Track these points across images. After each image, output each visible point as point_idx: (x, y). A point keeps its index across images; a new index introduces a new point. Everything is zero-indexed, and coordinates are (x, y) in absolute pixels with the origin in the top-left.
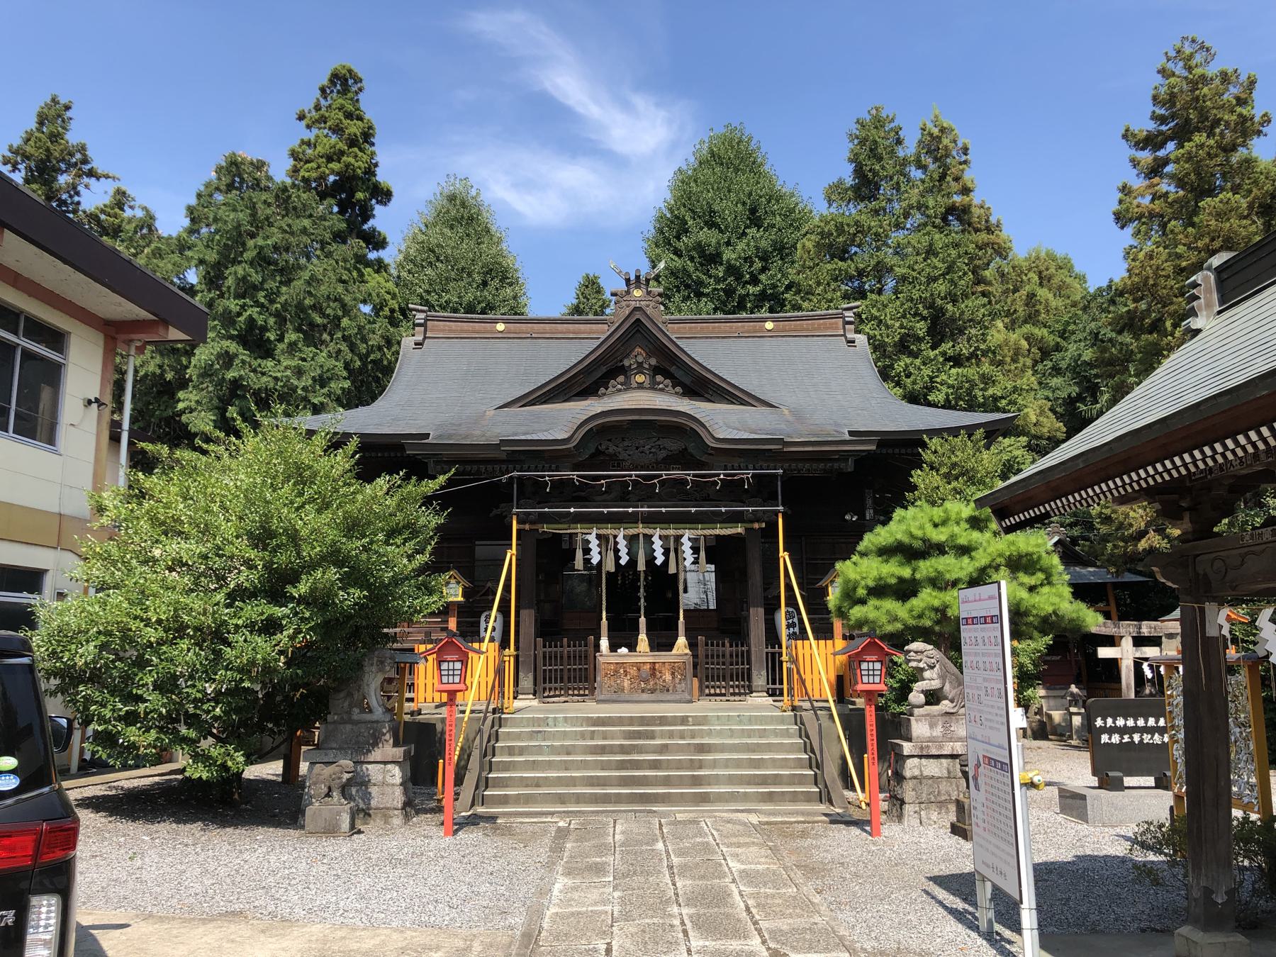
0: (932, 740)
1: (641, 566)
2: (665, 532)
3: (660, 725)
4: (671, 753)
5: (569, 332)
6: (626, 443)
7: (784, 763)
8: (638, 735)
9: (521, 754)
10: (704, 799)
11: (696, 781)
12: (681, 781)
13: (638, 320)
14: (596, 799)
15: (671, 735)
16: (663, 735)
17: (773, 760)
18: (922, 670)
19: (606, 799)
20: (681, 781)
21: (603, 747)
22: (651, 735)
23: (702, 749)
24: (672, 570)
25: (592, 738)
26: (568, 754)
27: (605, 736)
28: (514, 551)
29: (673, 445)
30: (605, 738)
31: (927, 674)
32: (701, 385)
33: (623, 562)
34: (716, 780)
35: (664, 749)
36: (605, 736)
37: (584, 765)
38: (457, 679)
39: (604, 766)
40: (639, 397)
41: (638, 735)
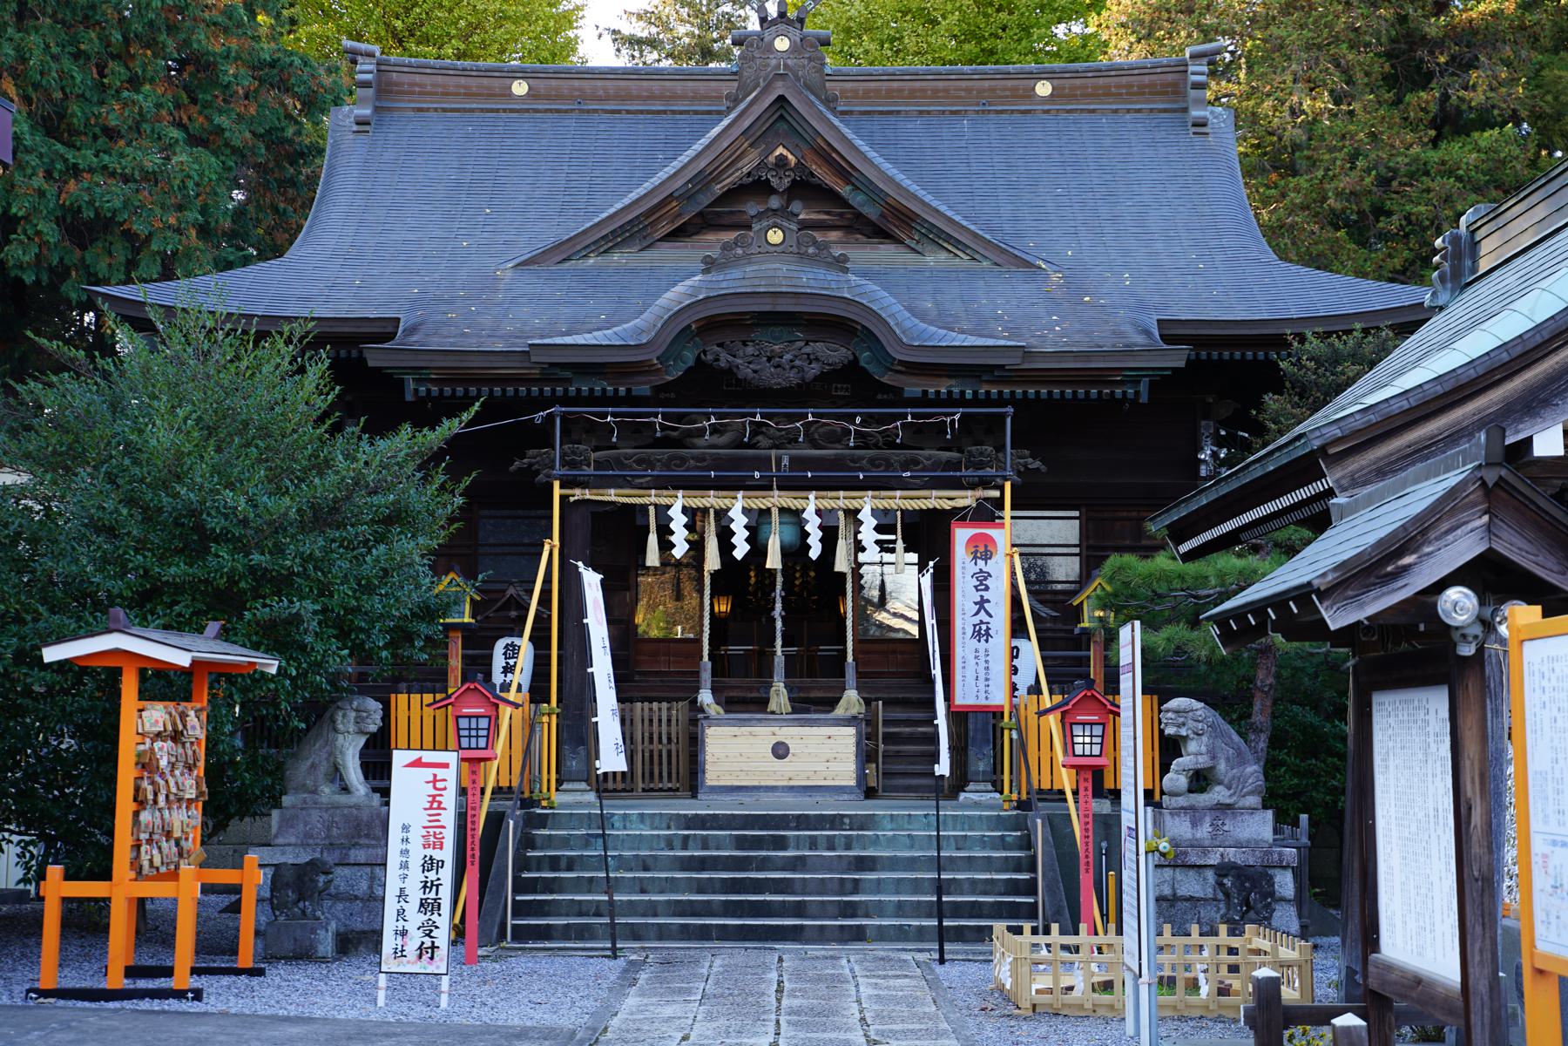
0: (1195, 844)
1: (774, 561)
2: (827, 504)
3: (797, 828)
4: (804, 870)
5: (652, 97)
6: (750, 350)
7: (988, 887)
8: (757, 843)
9: (570, 869)
10: (858, 935)
11: (849, 910)
12: (823, 910)
13: (781, 98)
14: (686, 933)
15: (813, 843)
16: (798, 843)
17: (973, 882)
18: (1186, 738)
19: (704, 934)
20: (823, 910)
21: (703, 859)
22: (780, 843)
23: (863, 864)
24: (842, 564)
25: (685, 848)
26: (646, 869)
27: (705, 843)
28: (556, 541)
29: (832, 353)
30: (705, 847)
31: (1192, 746)
32: (891, 223)
33: (739, 553)
34: (879, 909)
35: (797, 864)
36: (705, 843)
37: (672, 886)
38: (482, 742)
39: (701, 887)
40: (775, 261)
41: (757, 843)
